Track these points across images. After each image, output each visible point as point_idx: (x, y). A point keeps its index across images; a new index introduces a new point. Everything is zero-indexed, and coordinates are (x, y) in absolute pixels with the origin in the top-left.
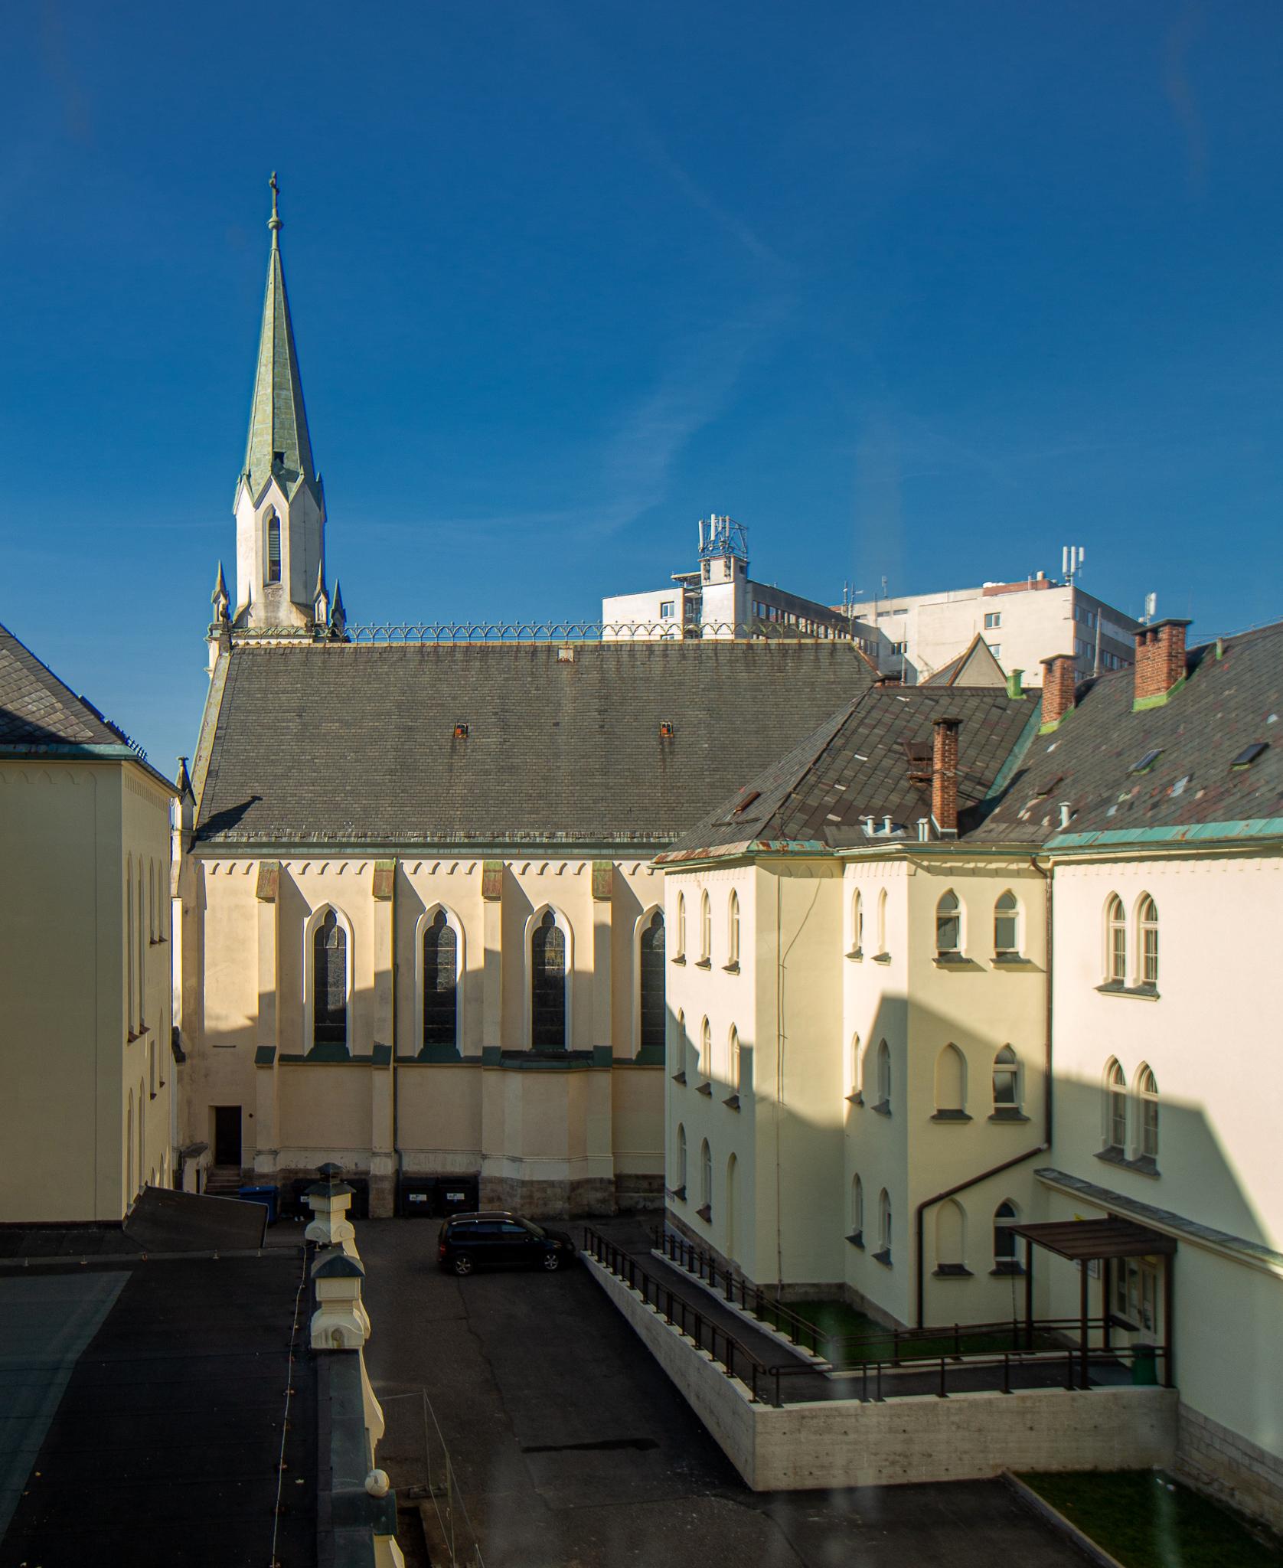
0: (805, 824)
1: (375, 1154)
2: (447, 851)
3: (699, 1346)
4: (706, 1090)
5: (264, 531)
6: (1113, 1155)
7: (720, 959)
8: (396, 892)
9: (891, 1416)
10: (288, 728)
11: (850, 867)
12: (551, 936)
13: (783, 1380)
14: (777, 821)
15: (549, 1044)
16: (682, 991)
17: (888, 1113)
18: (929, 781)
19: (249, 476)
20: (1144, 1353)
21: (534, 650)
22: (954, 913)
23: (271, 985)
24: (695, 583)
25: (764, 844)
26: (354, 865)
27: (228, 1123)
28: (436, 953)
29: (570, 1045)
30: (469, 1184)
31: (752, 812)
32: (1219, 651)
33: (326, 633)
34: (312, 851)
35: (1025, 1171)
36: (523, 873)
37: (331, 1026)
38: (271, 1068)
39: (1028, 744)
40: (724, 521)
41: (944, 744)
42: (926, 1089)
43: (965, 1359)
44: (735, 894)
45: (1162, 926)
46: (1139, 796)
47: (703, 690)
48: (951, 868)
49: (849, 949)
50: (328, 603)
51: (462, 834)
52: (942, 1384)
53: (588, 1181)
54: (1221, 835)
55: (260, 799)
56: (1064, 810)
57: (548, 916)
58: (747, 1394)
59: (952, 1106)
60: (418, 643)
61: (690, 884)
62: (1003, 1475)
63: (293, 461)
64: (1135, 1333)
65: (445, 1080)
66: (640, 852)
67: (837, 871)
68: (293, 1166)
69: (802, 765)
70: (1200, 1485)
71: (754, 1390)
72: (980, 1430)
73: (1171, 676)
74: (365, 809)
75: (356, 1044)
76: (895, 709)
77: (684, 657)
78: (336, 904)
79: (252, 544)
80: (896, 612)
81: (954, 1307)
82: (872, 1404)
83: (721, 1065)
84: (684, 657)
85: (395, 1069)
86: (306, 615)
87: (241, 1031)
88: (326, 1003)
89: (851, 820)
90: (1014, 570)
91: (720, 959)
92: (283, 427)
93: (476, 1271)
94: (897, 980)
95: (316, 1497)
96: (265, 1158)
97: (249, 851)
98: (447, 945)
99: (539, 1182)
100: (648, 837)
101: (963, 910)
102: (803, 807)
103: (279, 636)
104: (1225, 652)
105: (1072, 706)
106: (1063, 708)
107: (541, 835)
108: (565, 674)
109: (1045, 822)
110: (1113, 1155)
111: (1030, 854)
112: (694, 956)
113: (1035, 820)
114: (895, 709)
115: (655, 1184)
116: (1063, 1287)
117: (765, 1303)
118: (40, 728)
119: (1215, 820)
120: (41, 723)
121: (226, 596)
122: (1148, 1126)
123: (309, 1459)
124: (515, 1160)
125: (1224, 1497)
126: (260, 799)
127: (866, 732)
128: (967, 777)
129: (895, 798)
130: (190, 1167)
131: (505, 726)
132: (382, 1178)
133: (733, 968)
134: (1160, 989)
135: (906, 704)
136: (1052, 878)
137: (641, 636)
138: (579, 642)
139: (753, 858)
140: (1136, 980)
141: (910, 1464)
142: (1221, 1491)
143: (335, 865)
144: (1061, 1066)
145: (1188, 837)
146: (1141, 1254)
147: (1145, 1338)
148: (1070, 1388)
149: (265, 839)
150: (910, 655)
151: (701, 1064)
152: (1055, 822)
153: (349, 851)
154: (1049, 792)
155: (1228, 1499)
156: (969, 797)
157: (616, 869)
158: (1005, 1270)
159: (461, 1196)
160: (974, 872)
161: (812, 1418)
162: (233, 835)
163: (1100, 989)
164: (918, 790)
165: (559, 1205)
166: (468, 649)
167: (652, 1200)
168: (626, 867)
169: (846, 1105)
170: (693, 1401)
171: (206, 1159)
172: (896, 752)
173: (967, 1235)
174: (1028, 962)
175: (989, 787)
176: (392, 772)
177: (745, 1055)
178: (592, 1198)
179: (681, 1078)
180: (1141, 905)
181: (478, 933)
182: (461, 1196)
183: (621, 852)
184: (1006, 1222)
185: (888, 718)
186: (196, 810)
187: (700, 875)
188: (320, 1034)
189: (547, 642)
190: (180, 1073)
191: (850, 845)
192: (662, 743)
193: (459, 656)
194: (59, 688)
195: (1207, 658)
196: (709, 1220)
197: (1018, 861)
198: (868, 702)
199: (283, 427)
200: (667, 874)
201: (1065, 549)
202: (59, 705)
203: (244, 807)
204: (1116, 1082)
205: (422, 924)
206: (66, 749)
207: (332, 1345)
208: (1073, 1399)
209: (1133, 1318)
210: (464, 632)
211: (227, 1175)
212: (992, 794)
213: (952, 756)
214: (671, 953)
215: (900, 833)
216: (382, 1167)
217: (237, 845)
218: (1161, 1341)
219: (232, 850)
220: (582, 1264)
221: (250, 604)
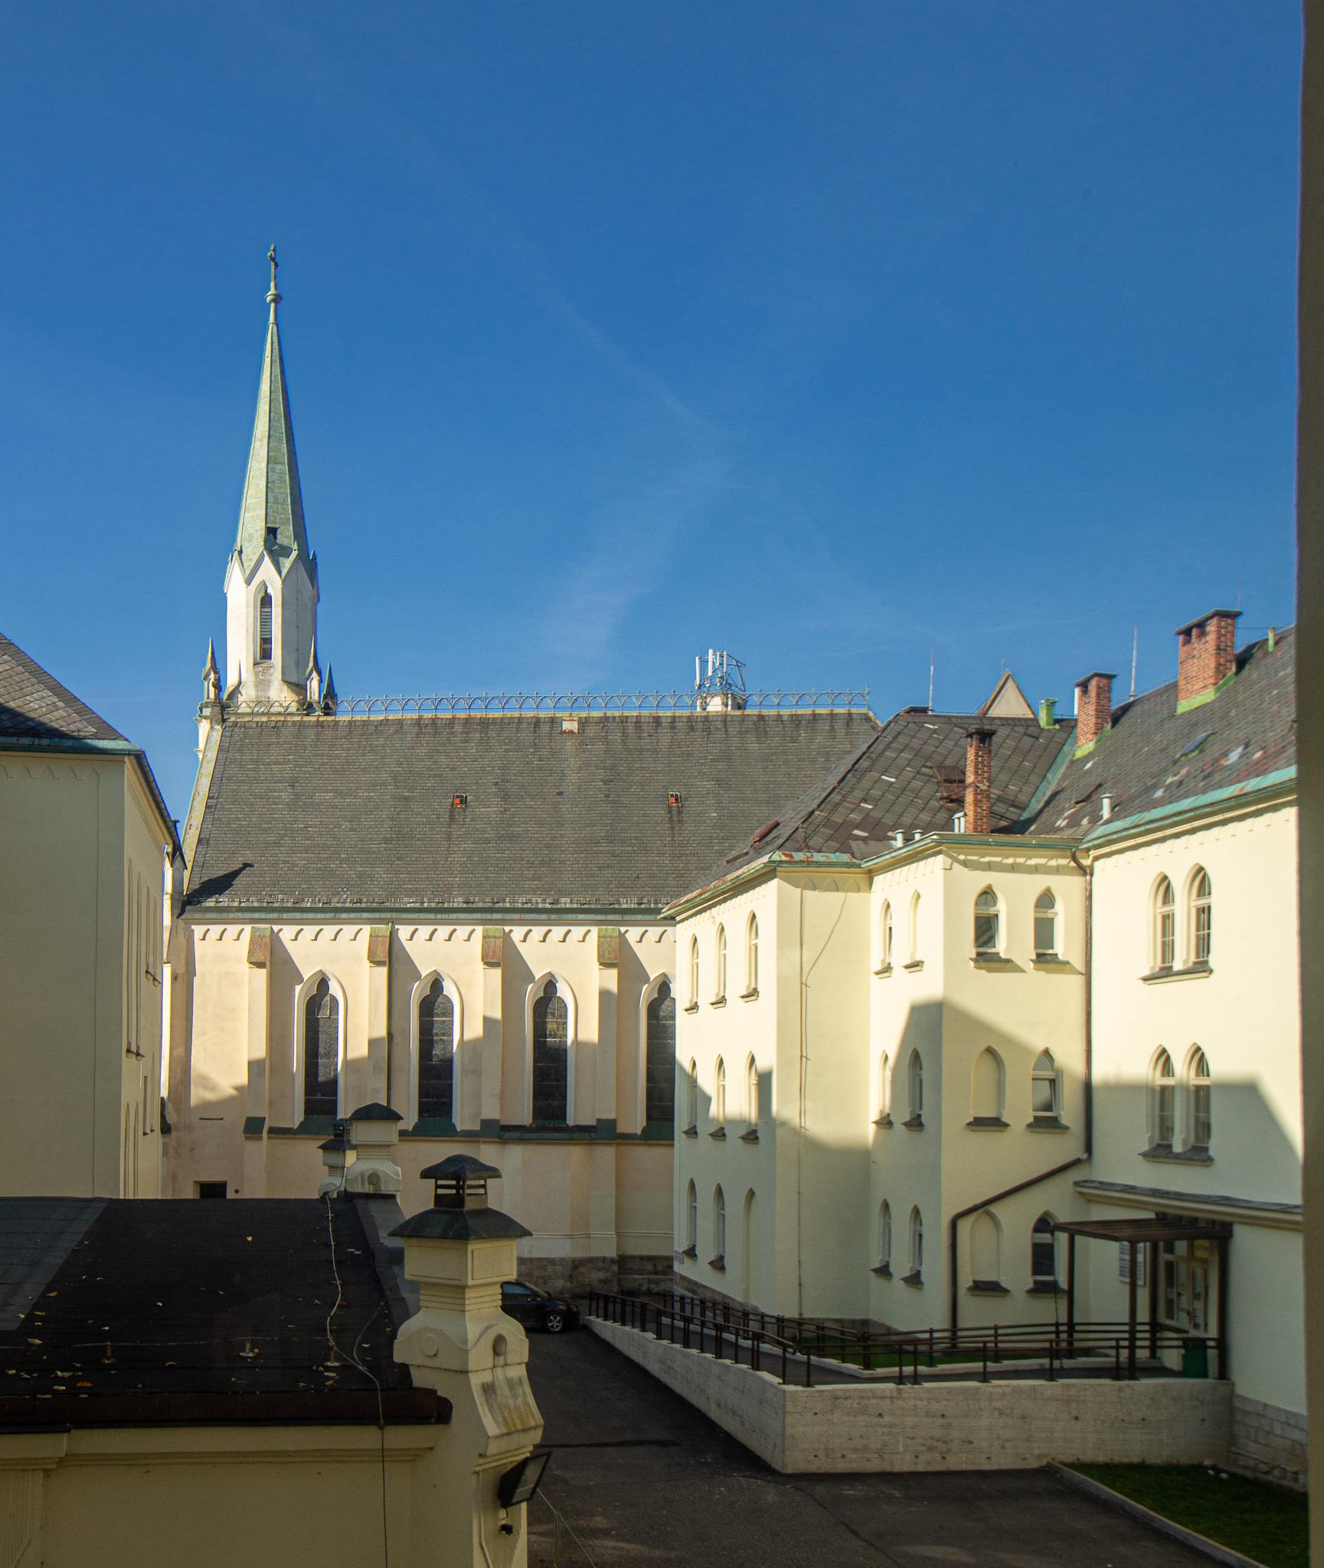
0: (831, 838)
2: (444, 916)
6: (1160, 1152)
8: (392, 958)
9: (929, 1400)
10: (280, 797)
11: (878, 880)
12: (553, 1005)
14: (801, 834)
16: (694, 1044)
17: (921, 1125)
19: (240, 552)
21: (537, 722)
22: (992, 911)
23: (261, 1052)
26: (349, 930)
29: (571, 1121)
32: (1271, 643)
34: (305, 916)
36: (524, 940)
37: (321, 1094)
38: (260, 1139)
39: (1062, 770)
40: (722, 656)
41: (977, 755)
42: (961, 1096)
44: (754, 917)
45: (1215, 901)
47: (712, 761)
48: (989, 863)
50: (321, 681)
53: (591, 1260)
55: (251, 866)
56: (1106, 803)
57: (550, 985)
58: (776, 1380)
60: (415, 716)
62: (1049, 1465)
63: (287, 536)
66: (647, 917)
67: (864, 884)
70: (1259, 1475)
72: (1024, 1417)
73: (1220, 671)
74: (360, 876)
76: (923, 735)
77: (692, 729)
78: (329, 971)
83: (734, 1101)
86: (298, 694)
87: (230, 1100)
88: (317, 1075)
94: (930, 986)
97: (240, 915)
98: (443, 1014)
99: (539, 1259)
100: (656, 903)
101: (1002, 908)
102: (827, 823)
104: (1276, 643)
105: (1108, 726)
106: (1099, 729)
107: (544, 901)
108: (570, 745)
109: (1085, 821)
110: (1160, 1152)
113: (1074, 822)
114: (923, 735)
119: (1277, 769)
120: (43, 719)
121: (216, 672)
125: (1285, 1483)
126: (251, 866)
127: (894, 755)
128: (999, 799)
129: (925, 817)
131: (505, 796)
134: (1212, 964)
135: (935, 731)
136: (1092, 875)
138: (584, 714)
139: (774, 870)
140: (1186, 961)
141: (949, 1450)
142: (1284, 1478)
143: (329, 930)
144: (1101, 1072)
151: (714, 1110)
152: (1096, 819)
153: (344, 915)
155: (1292, 1484)
156: (1002, 817)
157: (622, 936)
160: (1013, 868)
162: (224, 900)
164: (948, 809)
165: (560, 1284)
167: (657, 1283)
169: (871, 1130)
170: (714, 1414)
172: (924, 775)
174: (1067, 963)
176: (387, 841)
177: (764, 1082)
178: (595, 1277)
179: (692, 1132)
180: (1193, 881)
181: (475, 1001)
183: (627, 917)
185: (916, 743)
186: (187, 874)
188: (311, 1108)
189: (550, 714)
190: (164, 1145)
192: (670, 812)
193: (458, 728)
195: (1258, 653)
199: (276, 502)
202: (61, 704)
203: (235, 874)
204: (1163, 1075)
205: (417, 992)
206: (69, 743)
207: (368, 1189)
208: (1121, 1390)
209: (1182, 1321)
210: (462, 704)
212: (1025, 816)
217: (228, 910)
218: (1213, 1332)
219: (223, 915)
221: (240, 683)
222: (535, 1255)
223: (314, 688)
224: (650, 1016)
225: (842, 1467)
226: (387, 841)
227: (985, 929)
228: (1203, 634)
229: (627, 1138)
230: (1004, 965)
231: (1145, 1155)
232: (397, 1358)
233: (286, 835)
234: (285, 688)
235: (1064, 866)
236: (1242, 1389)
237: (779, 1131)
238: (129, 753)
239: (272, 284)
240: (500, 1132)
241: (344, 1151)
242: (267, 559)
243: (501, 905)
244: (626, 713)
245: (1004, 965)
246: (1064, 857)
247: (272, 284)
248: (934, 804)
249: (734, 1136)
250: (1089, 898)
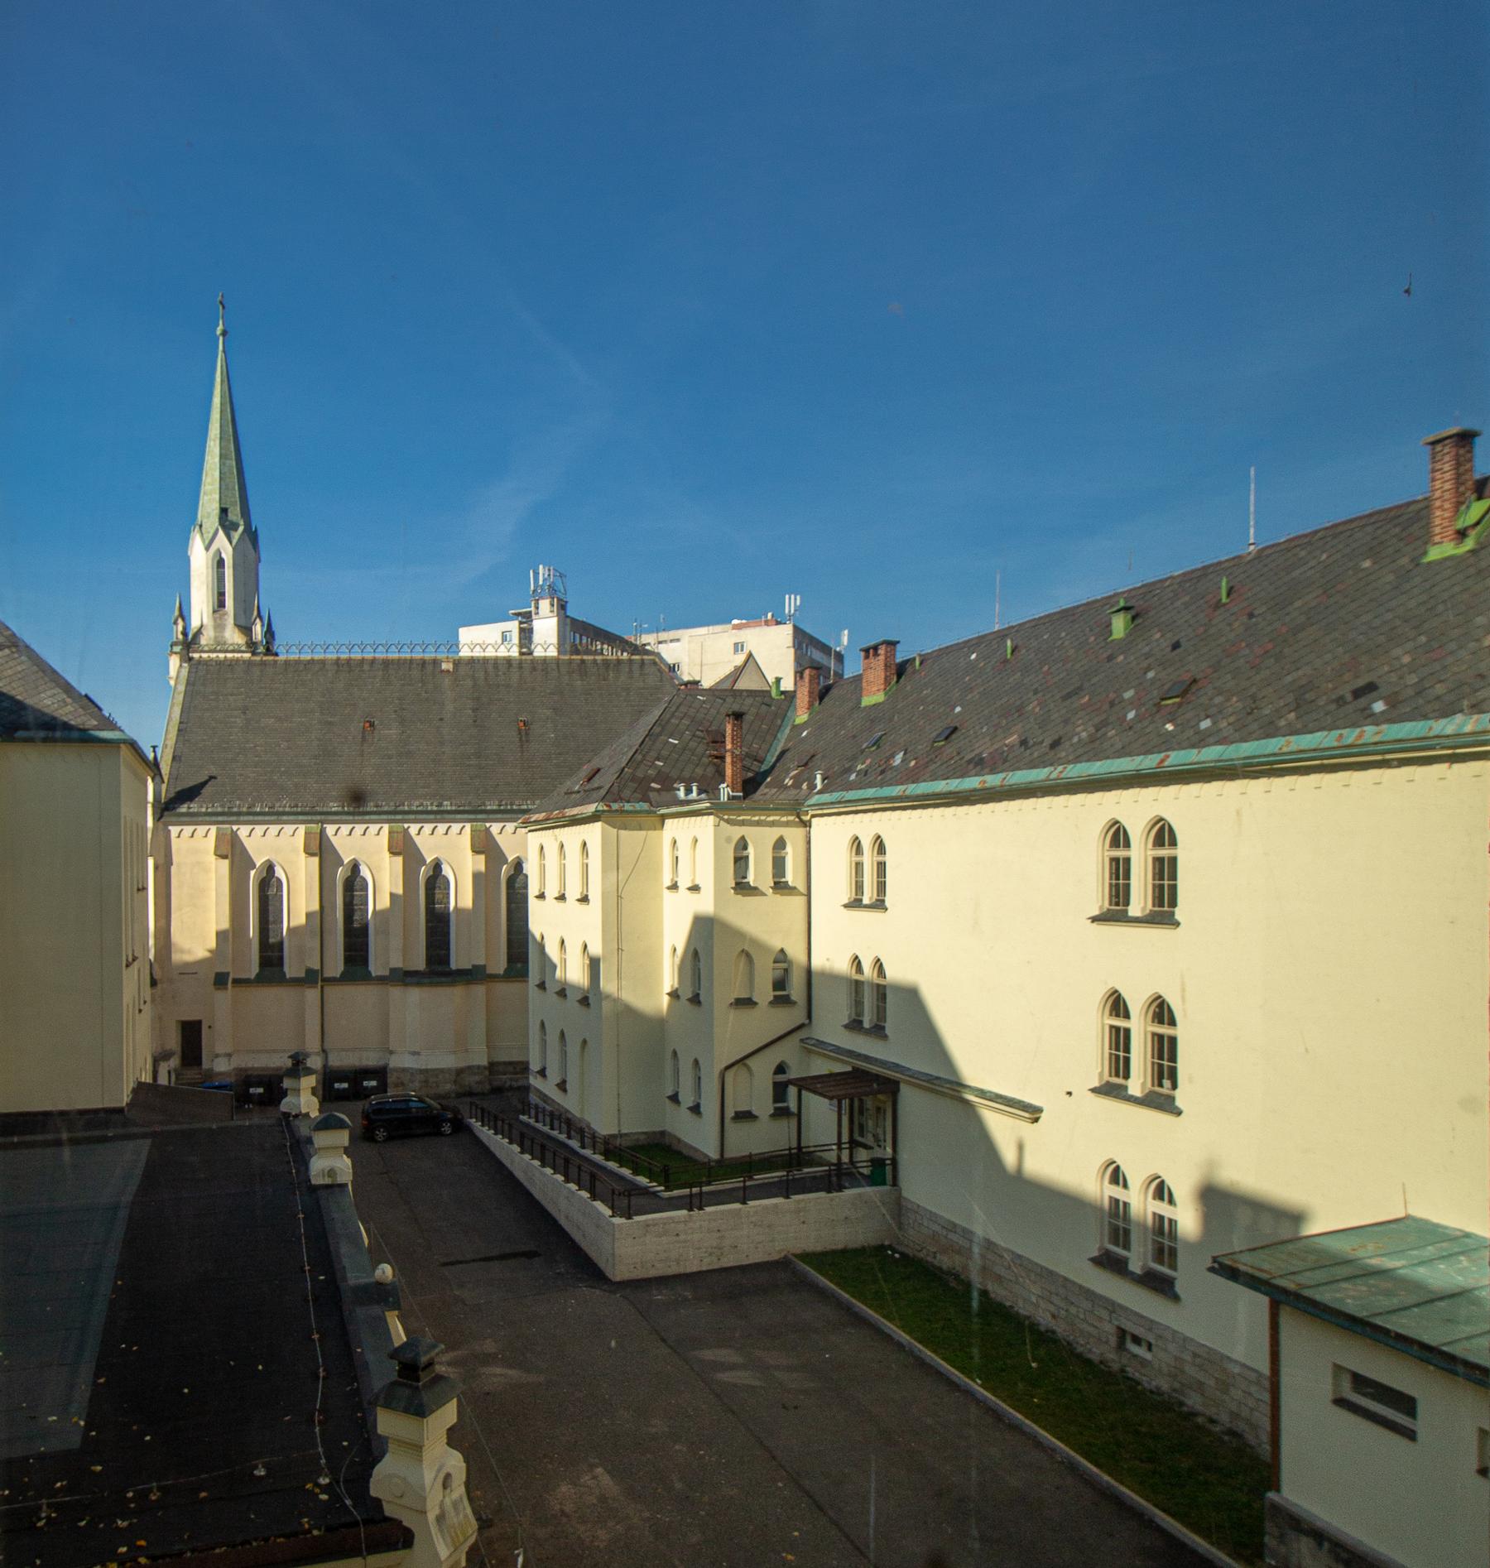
3: (567, 1181)
4: (562, 993)
6: (855, 1025)
7: (573, 893)
8: (321, 849)
11: (668, 822)
12: (439, 882)
13: (627, 1200)
15: (438, 967)
16: (543, 920)
17: (699, 1003)
18: (722, 758)
20: (878, 1163)
21: (423, 663)
23: (225, 924)
24: (527, 618)
26: (289, 829)
27: (191, 1032)
28: (352, 897)
29: (453, 966)
30: (380, 1073)
31: (596, 783)
33: (261, 649)
37: (271, 956)
39: (787, 731)
42: (726, 985)
45: (889, 859)
46: (870, 766)
49: (669, 884)
52: (744, 1196)
53: (469, 1068)
54: (930, 791)
58: (608, 1212)
59: (744, 995)
61: (548, 839)
63: (235, 515)
65: (361, 995)
69: (630, 747)
71: (612, 1208)
73: (887, 681)
75: (291, 969)
77: (534, 669)
79: (203, 578)
81: (747, 1142)
82: (696, 1212)
83: (574, 973)
84: (534, 669)
89: (668, 785)
90: (757, 610)
91: (573, 893)
93: (390, 1138)
94: (705, 904)
95: (338, 1288)
96: (221, 1061)
101: (751, 851)
102: (633, 779)
103: (227, 651)
106: (811, 705)
108: (447, 681)
109: (805, 786)
110: (855, 1025)
112: (552, 891)
113: (797, 785)
115: (523, 1068)
116: (822, 1121)
117: (610, 1148)
118: (54, 718)
120: (56, 714)
122: (881, 1003)
123: (325, 1259)
124: (415, 1053)
128: (747, 755)
129: (699, 771)
130: (163, 1069)
133: (584, 899)
134: (887, 904)
137: (490, 653)
144: (817, 962)
145: (908, 793)
146: (874, 1093)
147: (878, 1153)
148: (829, 1192)
151: (558, 973)
152: (812, 786)
154: (806, 765)
156: (749, 770)
158: (781, 1113)
159: (374, 1083)
160: (758, 824)
162: (194, 807)
163: (846, 906)
165: (448, 1087)
168: (495, 828)
169: (666, 1000)
170: (563, 1222)
171: (174, 1062)
173: (755, 1091)
176: (316, 757)
177: (594, 964)
178: (471, 1080)
179: (542, 986)
181: (384, 881)
182: (374, 1083)
184: (781, 1078)
185: (692, 712)
186: (164, 787)
187: (557, 831)
191: (668, 806)
193: (366, 667)
194: (68, 689)
195: (909, 670)
196: (565, 1091)
198: (677, 700)
203: (205, 783)
205: (341, 873)
207: (328, 1181)
209: (869, 1140)
211: (191, 1074)
212: (764, 767)
214: (533, 890)
215: (703, 796)
219: (194, 819)
220: (469, 1130)
223: (258, 630)
224: (510, 890)
225: (652, 1273)
226: (316, 757)
228: (876, 654)
229: (494, 977)
230: (752, 891)
231: (846, 1026)
232: (373, 1493)
236: (905, 1194)
237: (604, 1003)
238: (125, 742)
240: (405, 977)
242: (221, 532)
245: (752, 891)
248: (705, 760)
249: (573, 997)
250: (809, 842)
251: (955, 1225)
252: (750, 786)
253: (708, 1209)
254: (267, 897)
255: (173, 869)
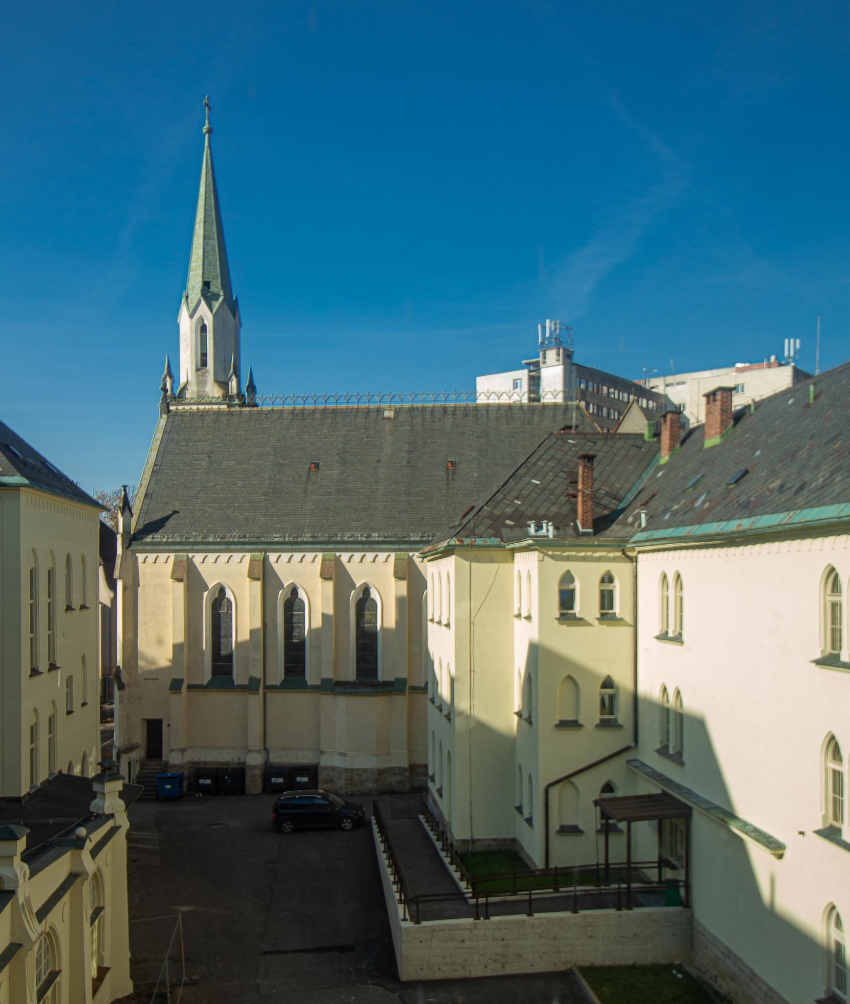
0: (490, 527)
1: (249, 751)
5: (196, 333)
6: (663, 751)
8: (264, 574)
10: (200, 465)
12: (368, 603)
14: (471, 524)
18: (575, 497)
19: (187, 297)
21: (368, 411)
22: (571, 586)
23: (181, 639)
25: (459, 540)
26: (237, 556)
28: (292, 616)
29: (381, 678)
30: (312, 771)
32: (753, 408)
34: (209, 547)
35: (621, 760)
36: (349, 561)
37: (222, 664)
38: (180, 693)
40: (555, 324)
41: (584, 472)
43: (562, 889)
45: (685, 594)
49: (516, 612)
51: (309, 535)
52: (530, 908)
53: (391, 769)
55: (178, 512)
57: (366, 590)
60: (291, 407)
62: (571, 969)
63: (216, 287)
64: (676, 871)
65: (297, 702)
68: (197, 760)
72: (555, 938)
73: (723, 424)
75: (239, 677)
77: (466, 415)
78: (225, 582)
79: (188, 342)
80: (678, 384)
81: (573, 854)
85: (265, 694)
88: (219, 649)
92: (210, 265)
93: (296, 830)
97: (167, 547)
101: (577, 585)
102: (491, 516)
105: (678, 445)
106: (672, 448)
107: (362, 536)
108: (388, 427)
110: (663, 751)
111: (619, 546)
119: (706, 523)
121: (171, 377)
122: (683, 733)
126: (178, 512)
129: (554, 509)
132: (254, 767)
135: (574, 445)
137: (504, 400)
138: (398, 405)
141: (507, 962)
143: (224, 556)
144: (643, 689)
148: (619, 909)
149: (178, 540)
150: (686, 413)
153: (233, 547)
156: (606, 507)
159: (305, 779)
160: (585, 559)
161: (441, 931)
162: (157, 537)
165: (371, 785)
166: (324, 411)
171: (138, 755)
175: (621, 501)
181: (318, 603)
182: (305, 779)
185: (559, 455)
192: (447, 473)
193: (317, 416)
197: (614, 551)
198: (547, 444)
199: (210, 265)
200: (429, 561)
201: (786, 341)
203: (167, 518)
205: (281, 596)
208: (620, 917)
211: (153, 765)
212: (622, 505)
213: (590, 480)
216: (255, 760)
217: (160, 544)
218: (683, 878)
219: (156, 548)
222: (354, 767)
225: (439, 975)
227: (567, 599)
230: (579, 621)
233: (202, 491)
234: (216, 386)
235: (618, 557)
239: (207, 122)
241: (103, 784)
242: (203, 303)
243: (334, 539)
244: (426, 405)
245: (579, 621)
246: (618, 551)
247: (207, 122)
250: (636, 577)
251: (730, 951)
252: (601, 524)
253: (494, 919)
254: (219, 614)
255: (140, 590)
